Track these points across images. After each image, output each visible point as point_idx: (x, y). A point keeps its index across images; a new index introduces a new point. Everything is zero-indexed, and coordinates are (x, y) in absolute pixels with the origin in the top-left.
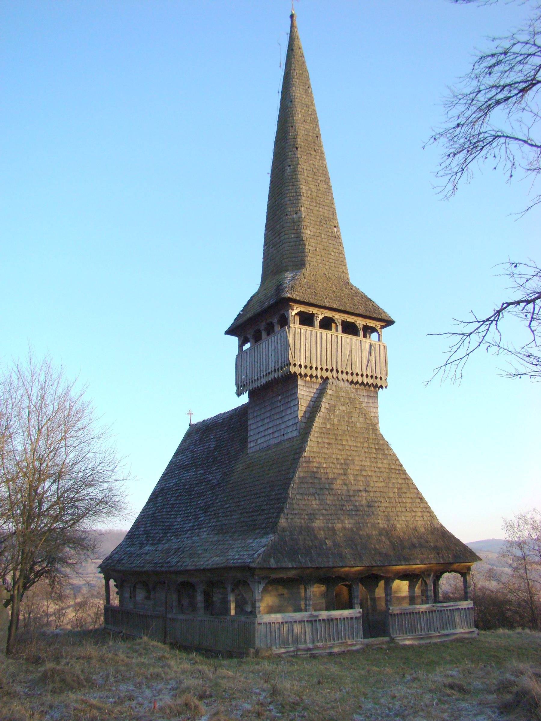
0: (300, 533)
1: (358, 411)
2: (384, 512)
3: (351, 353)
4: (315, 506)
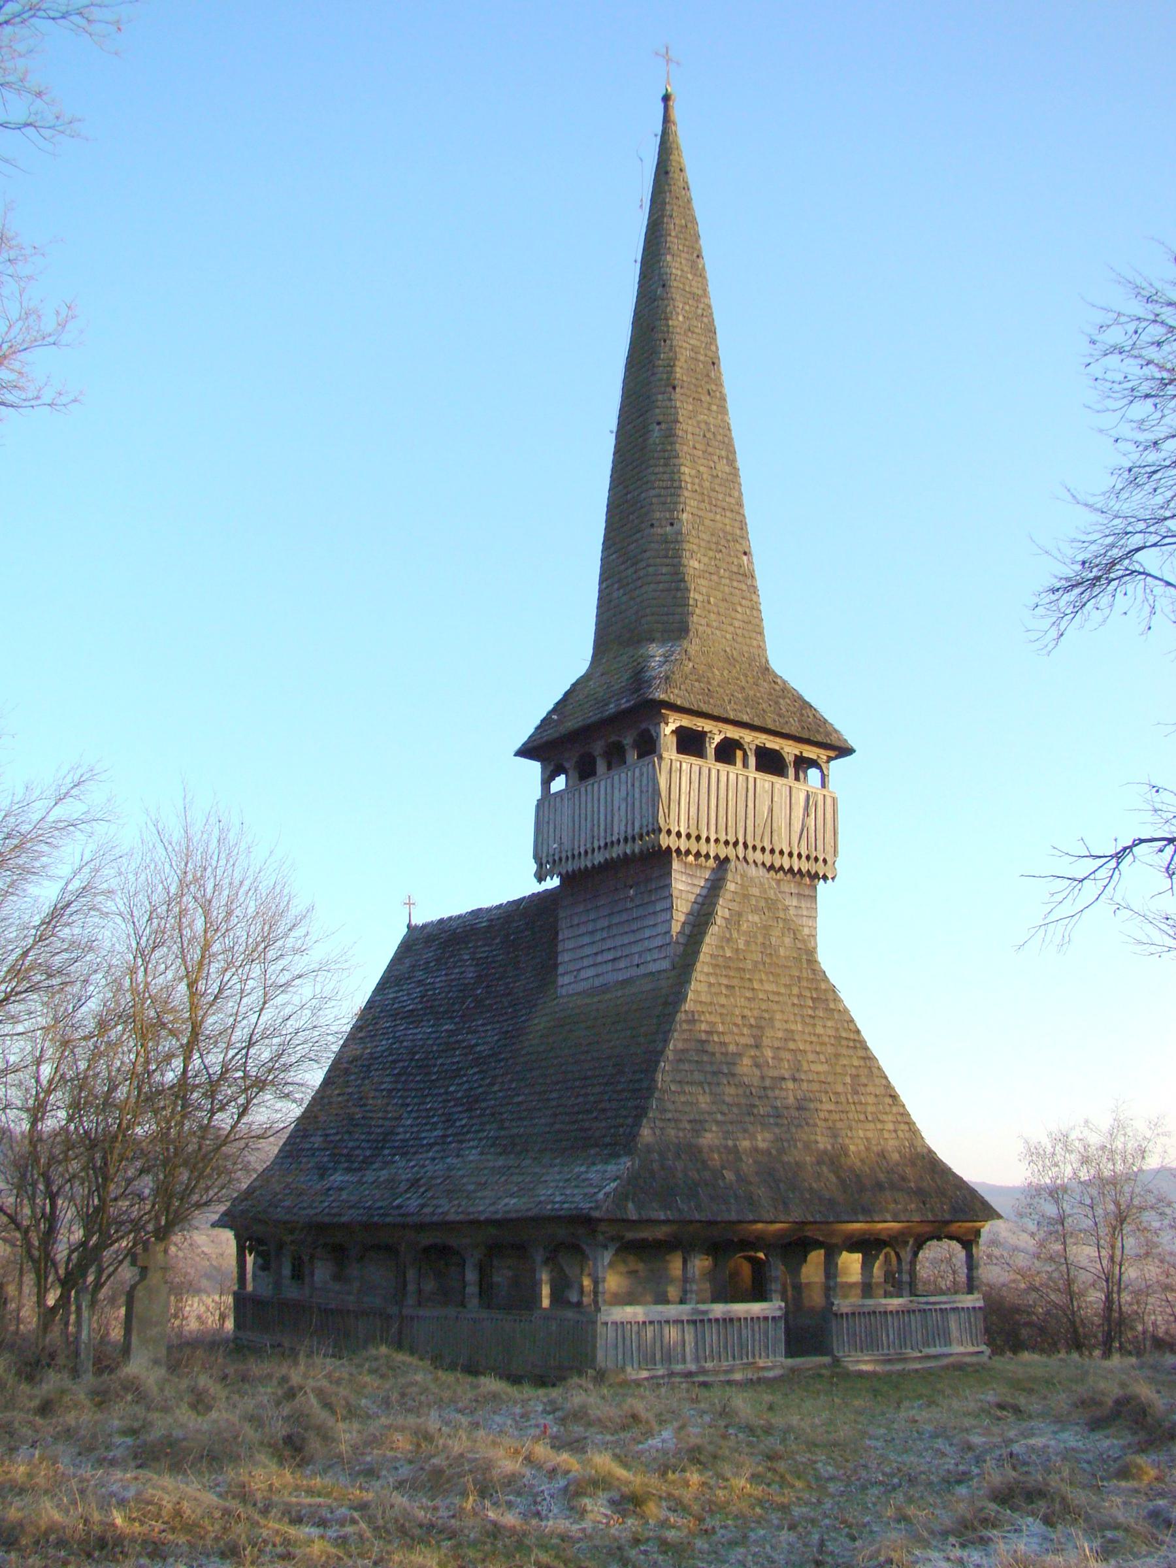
0: (678, 1156)
1: (781, 925)
2: (826, 1120)
3: (771, 810)
4: (703, 1105)
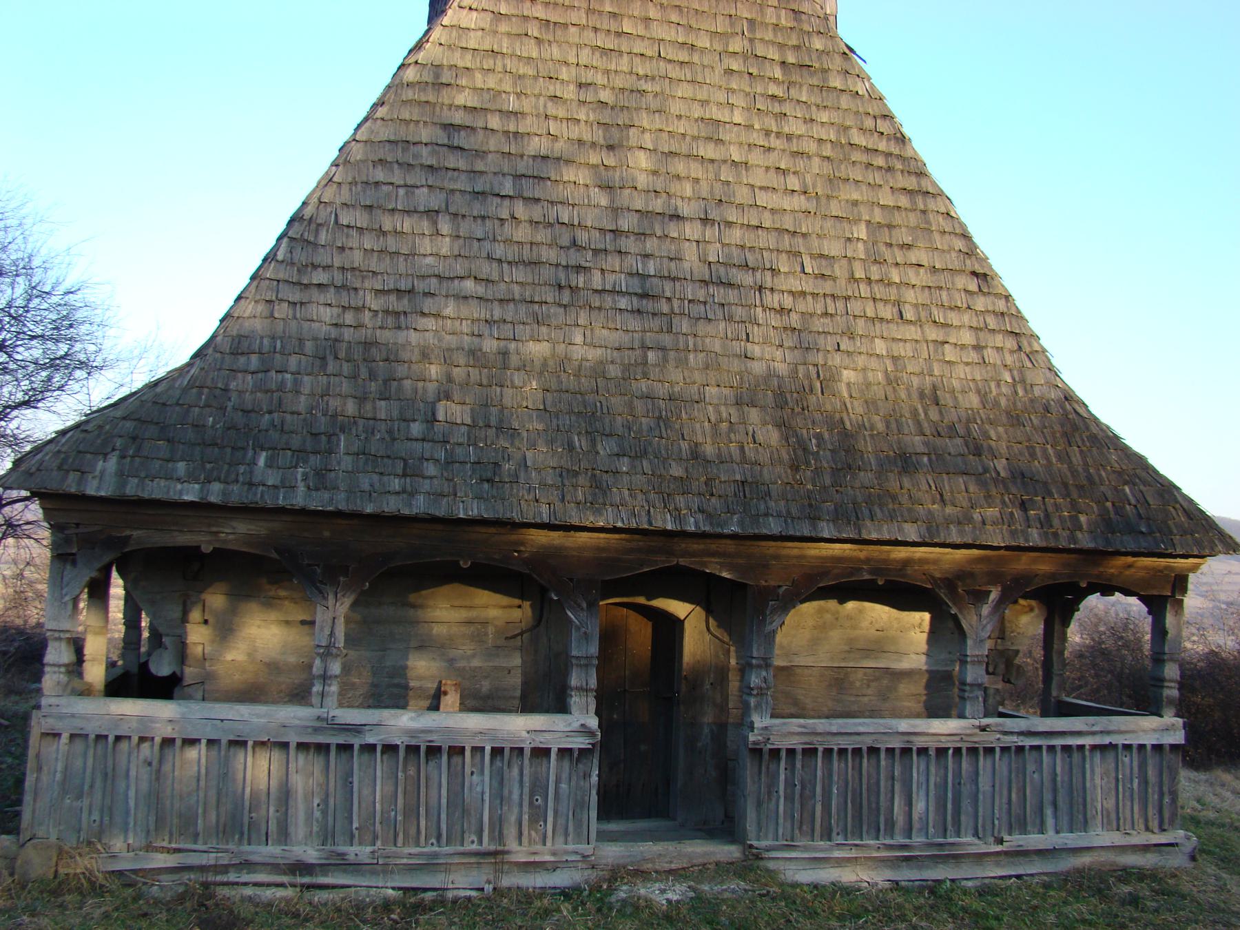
2: (782, 311)
